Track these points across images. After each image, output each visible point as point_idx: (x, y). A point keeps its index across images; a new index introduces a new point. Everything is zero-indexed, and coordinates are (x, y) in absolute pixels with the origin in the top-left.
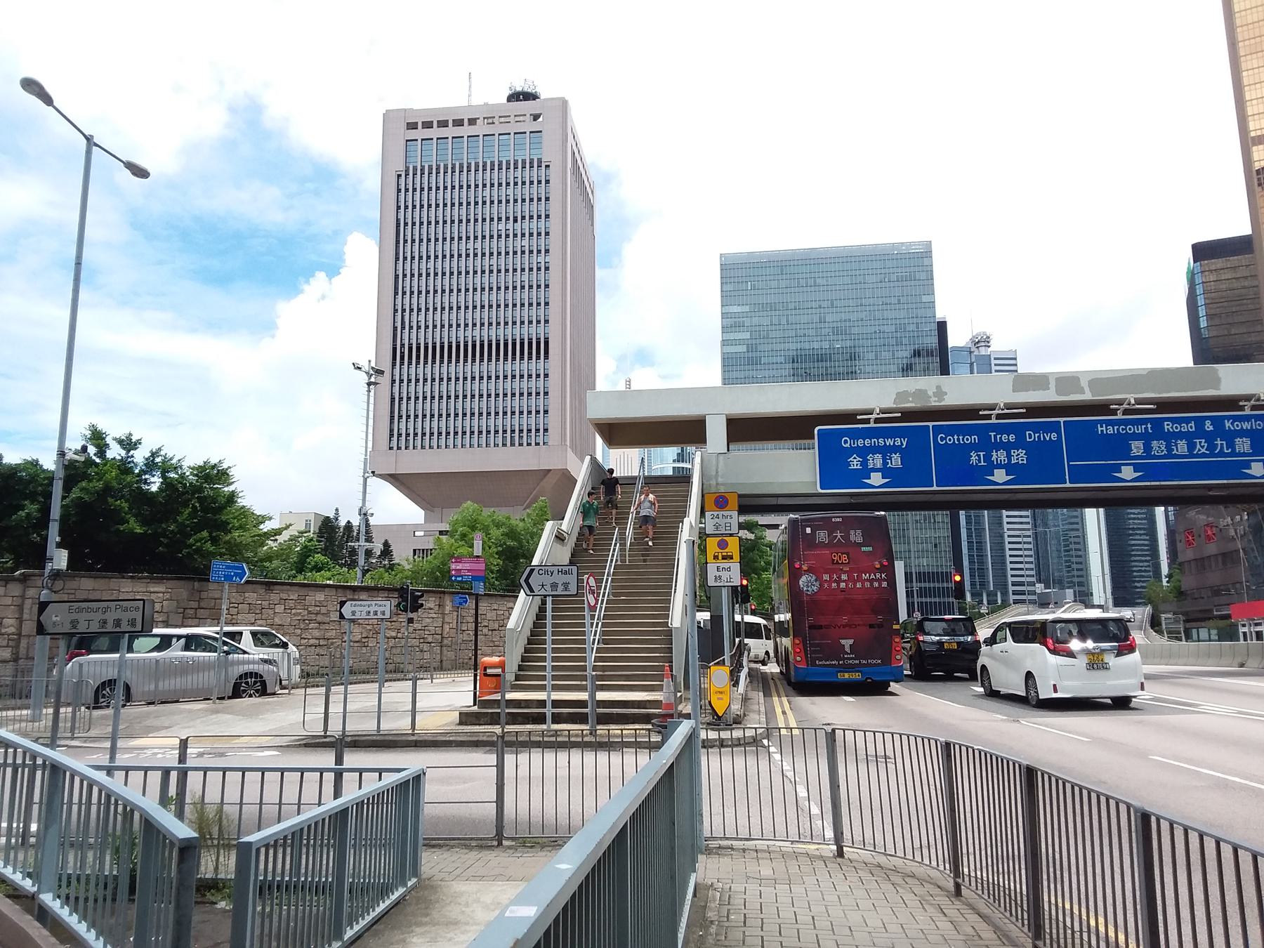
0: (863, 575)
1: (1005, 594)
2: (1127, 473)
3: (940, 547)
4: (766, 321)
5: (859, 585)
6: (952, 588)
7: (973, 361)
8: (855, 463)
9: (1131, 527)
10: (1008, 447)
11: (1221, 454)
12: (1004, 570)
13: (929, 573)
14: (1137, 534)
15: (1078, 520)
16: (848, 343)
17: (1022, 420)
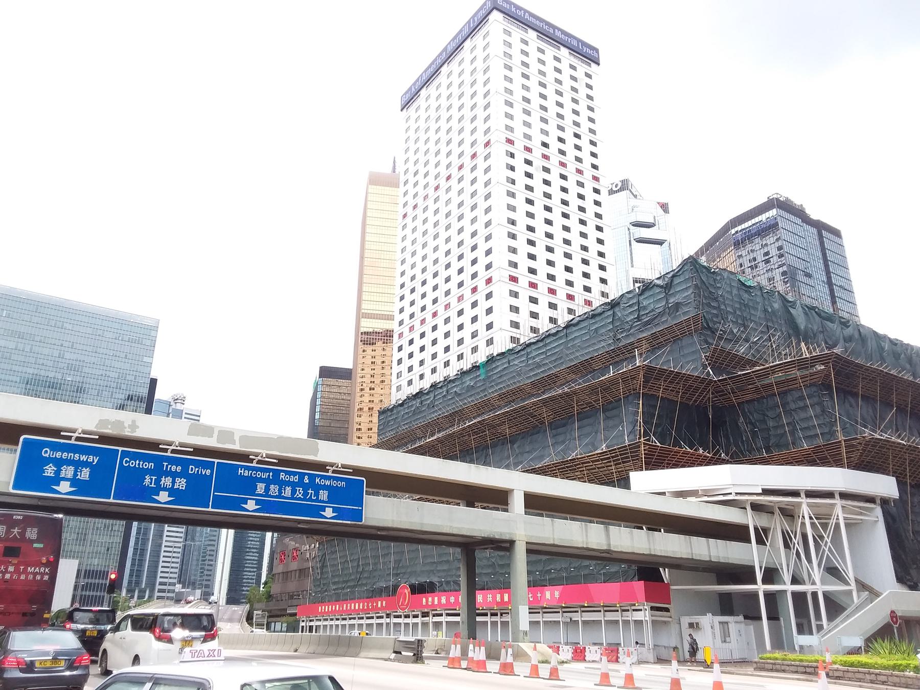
0: (29, 568)
2: (251, 505)
3: (111, 551)
4: (12, 345)
5: (23, 577)
6: (106, 584)
8: (50, 471)
9: (249, 546)
10: (174, 475)
11: (310, 500)
12: (156, 572)
13: (104, 572)
14: (251, 552)
15: (216, 538)
16: (78, 379)
17: (189, 457)
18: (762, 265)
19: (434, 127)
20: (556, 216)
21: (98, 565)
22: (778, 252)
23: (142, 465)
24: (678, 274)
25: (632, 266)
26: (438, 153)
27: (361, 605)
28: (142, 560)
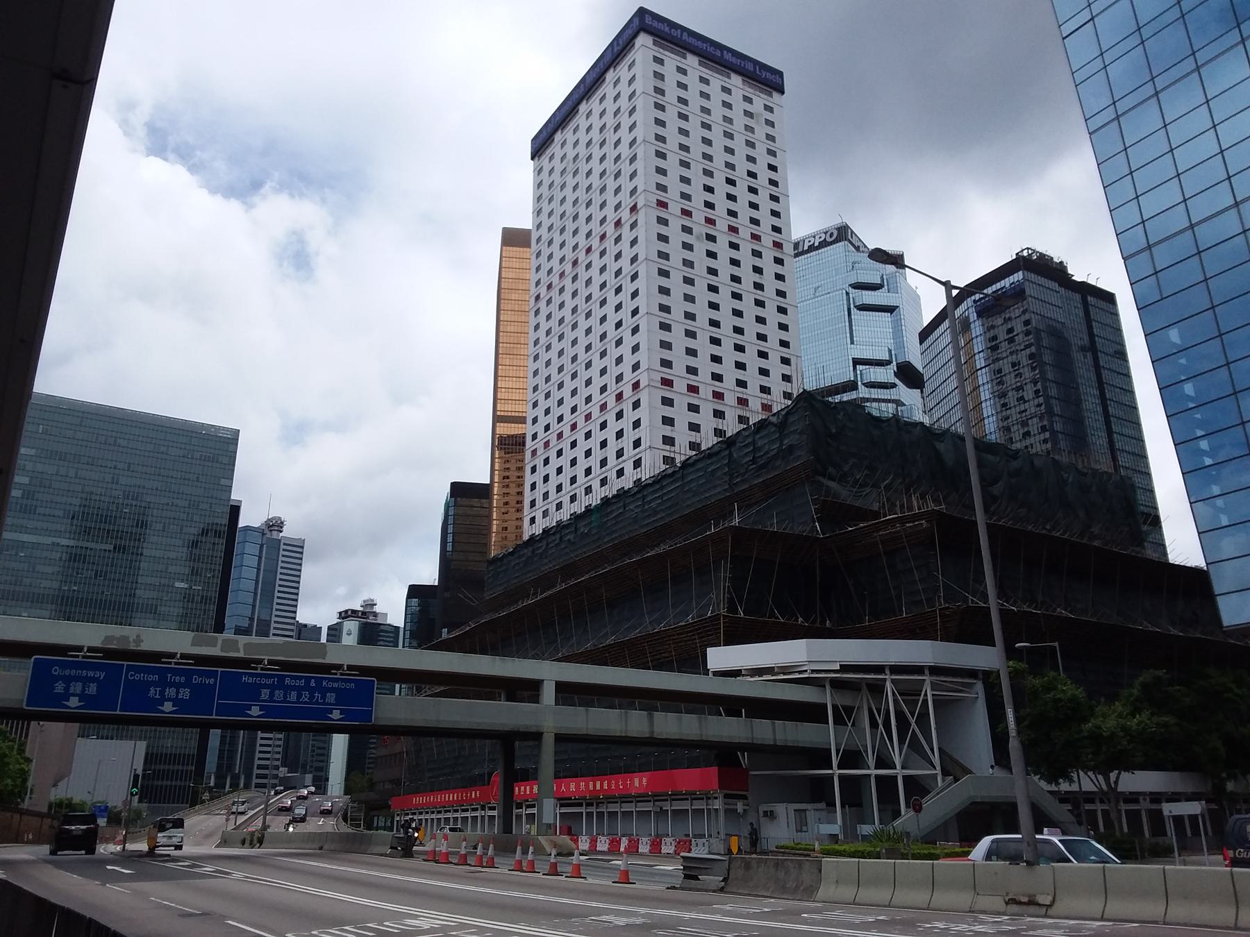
1: (249, 777)
2: (255, 711)
7: (264, 542)
8: (59, 688)
10: (178, 686)
11: (317, 702)
18: (1004, 345)
19: (597, 154)
20: (723, 298)
21: (172, 746)
22: (1024, 329)
23: (147, 678)
24: (793, 411)
25: (852, 343)
26: (603, 190)
27: (455, 795)
28: (235, 737)
